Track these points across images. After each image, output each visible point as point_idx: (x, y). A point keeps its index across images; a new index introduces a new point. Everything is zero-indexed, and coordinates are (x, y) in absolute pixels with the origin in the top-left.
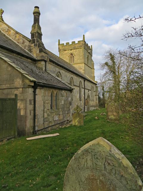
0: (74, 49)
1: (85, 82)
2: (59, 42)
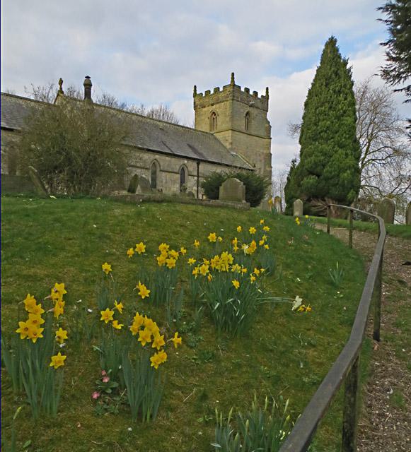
0: (218, 103)
1: (200, 166)
2: (195, 90)
